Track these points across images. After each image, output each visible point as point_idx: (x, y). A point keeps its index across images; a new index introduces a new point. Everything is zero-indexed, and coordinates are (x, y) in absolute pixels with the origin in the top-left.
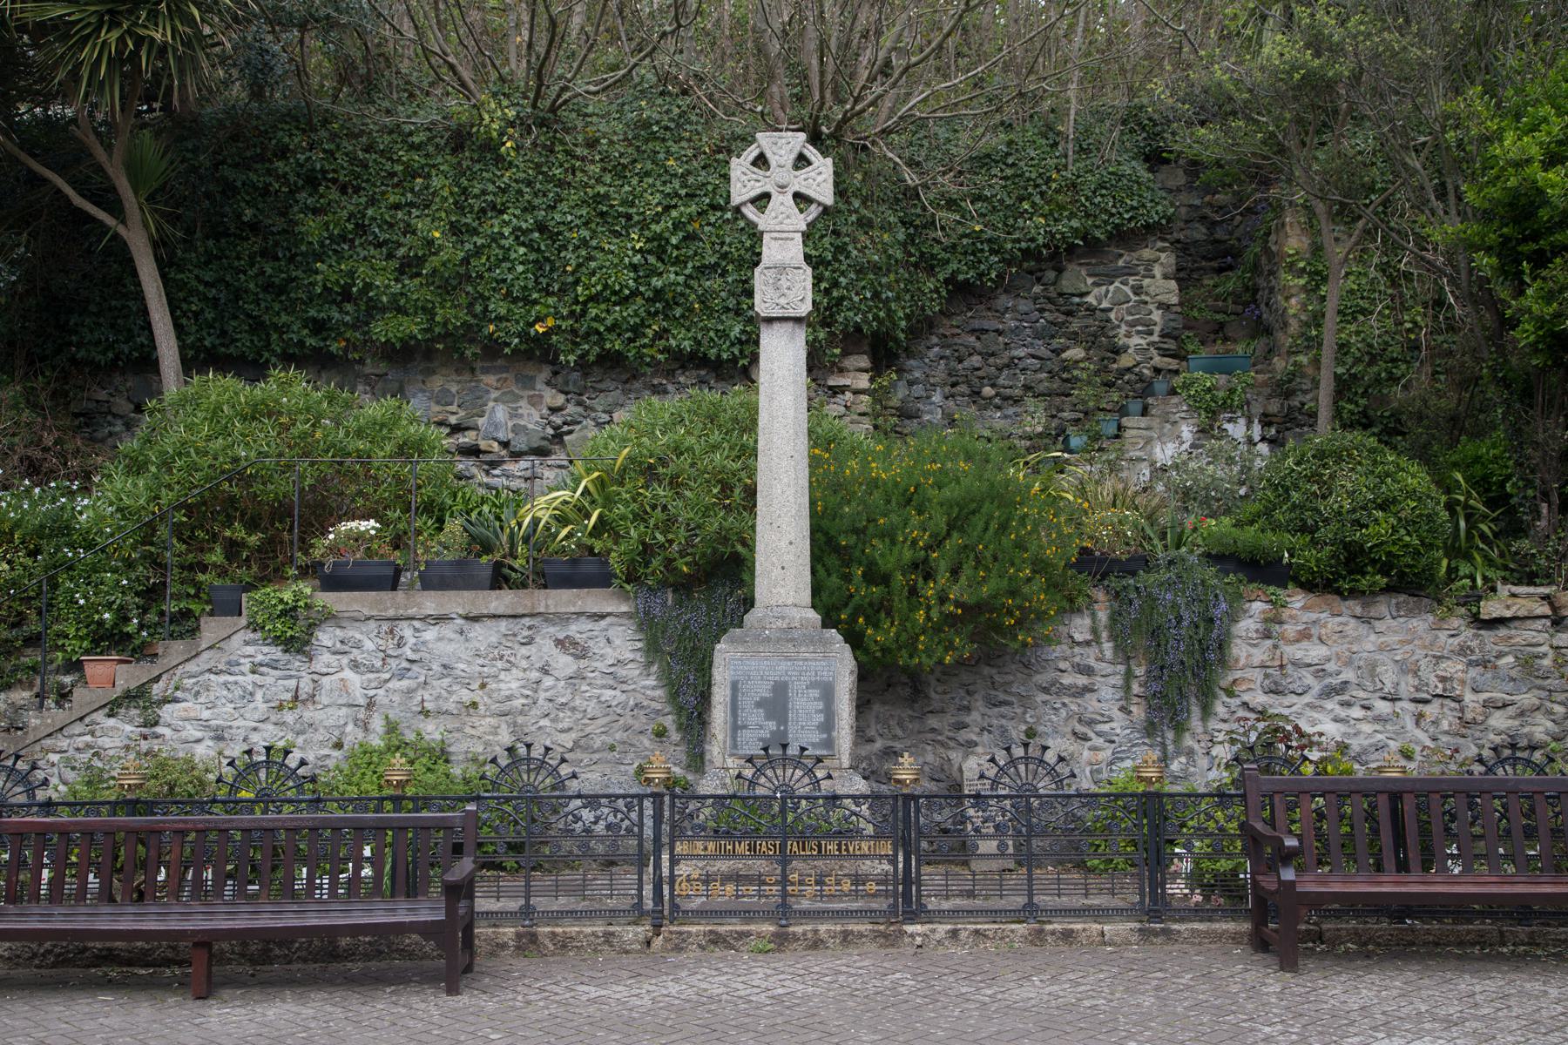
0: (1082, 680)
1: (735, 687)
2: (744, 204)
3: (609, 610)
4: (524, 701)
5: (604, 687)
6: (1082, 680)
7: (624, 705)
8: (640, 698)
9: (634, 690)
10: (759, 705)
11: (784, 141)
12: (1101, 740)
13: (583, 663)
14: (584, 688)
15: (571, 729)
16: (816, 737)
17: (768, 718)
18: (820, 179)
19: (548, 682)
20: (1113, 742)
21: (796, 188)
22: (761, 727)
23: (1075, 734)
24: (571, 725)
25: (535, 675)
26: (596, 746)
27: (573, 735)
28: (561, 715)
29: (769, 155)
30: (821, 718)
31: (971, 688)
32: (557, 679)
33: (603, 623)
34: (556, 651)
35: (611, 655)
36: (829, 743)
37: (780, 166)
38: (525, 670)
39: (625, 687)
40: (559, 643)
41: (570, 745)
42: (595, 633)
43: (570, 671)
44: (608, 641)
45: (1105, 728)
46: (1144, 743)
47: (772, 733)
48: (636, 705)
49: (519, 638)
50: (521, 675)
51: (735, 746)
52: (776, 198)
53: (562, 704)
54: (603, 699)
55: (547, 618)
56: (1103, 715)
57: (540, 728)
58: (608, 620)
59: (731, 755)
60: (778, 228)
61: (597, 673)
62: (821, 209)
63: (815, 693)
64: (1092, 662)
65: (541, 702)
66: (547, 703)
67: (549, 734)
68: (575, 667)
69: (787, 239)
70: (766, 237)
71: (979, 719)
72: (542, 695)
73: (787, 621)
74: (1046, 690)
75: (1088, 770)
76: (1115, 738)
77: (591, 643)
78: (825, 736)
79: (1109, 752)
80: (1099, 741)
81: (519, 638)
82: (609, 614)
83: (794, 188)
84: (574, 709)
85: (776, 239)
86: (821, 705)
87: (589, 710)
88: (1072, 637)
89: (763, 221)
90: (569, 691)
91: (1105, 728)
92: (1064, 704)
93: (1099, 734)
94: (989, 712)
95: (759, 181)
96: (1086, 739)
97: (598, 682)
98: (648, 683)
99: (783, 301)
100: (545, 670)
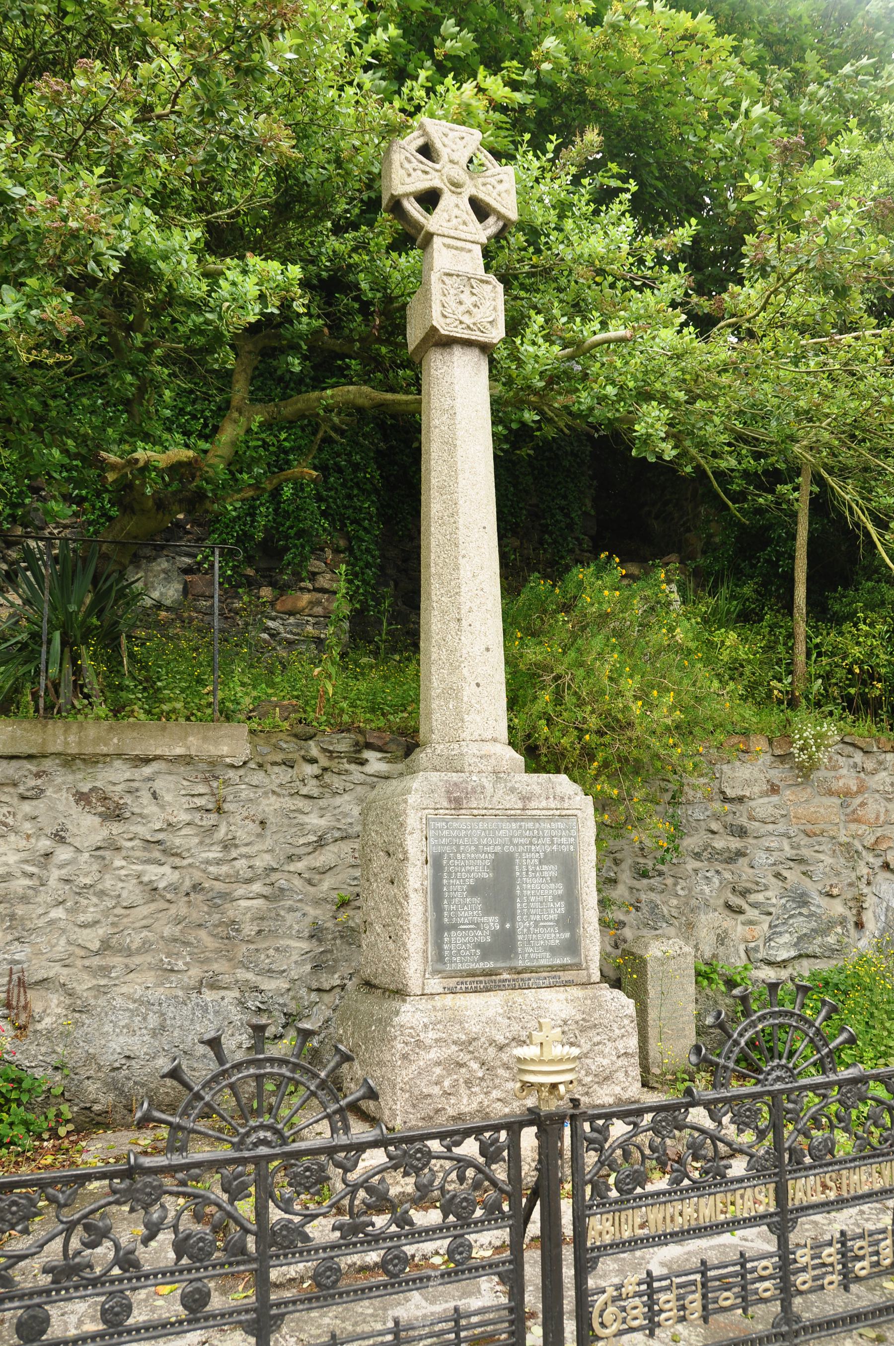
0: (735, 843)
1: (437, 864)
2: (407, 195)
3: (158, 752)
4: (28, 882)
5: (148, 861)
6: (735, 843)
7: (174, 888)
8: (198, 876)
9: (190, 865)
10: (473, 891)
11: (457, 134)
12: (756, 912)
13: (116, 828)
14: (118, 863)
15: (97, 922)
16: (557, 937)
17: (487, 912)
18: (500, 187)
19: (63, 854)
20: (770, 914)
21: (474, 192)
22: (478, 926)
23: (728, 906)
24: (98, 917)
25: (45, 844)
26: (134, 947)
27: (101, 931)
28: (84, 902)
29: (438, 145)
30: (560, 908)
31: (618, 855)
32: (78, 850)
33: (147, 770)
34: (75, 810)
35: (156, 817)
36: (572, 946)
37: (451, 161)
38: (28, 836)
39: (177, 861)
40: (82, 798)
41: (96, 945)
42: (135, 785)
43: (97, 838)
44: (155, 795)
45: (760, 897)
46: (800, 914)
47: (494, 934)
48: (194, 887)
49: (21, 789)
50: (23, 843)
51: (440, 957)
52: (447, 201)
53: (85, 886)
54: (146, 879)
55: (69, 761)
56: (757, 883)
57: (51, 922)
58: (155, 766)
59: (435, 972)
60: (452, 233)
61: (136, 842)
62: (501, 224)
63: (551, 870)
64: (744, 821)
65: (53, 882)
66: (61, 885)
67: (64, 931)
68: (105, 833)
69: (462, 249)
70: (437, 242)
71: (627, 894)
72: (55, 874)
73: (493, 761)
74: (697, 856)
75: (742, 948)
76: (772, 910)
77: (128, 799)
78: (567, 935)
79: (766, 926)
80: (752, 913)
81: (21, 789)
82: (156, 758)
83: (469, 190)
84: (102, 894)
85: (448, 247)
86: (559, 889)
87: (125, 894)
88: (723, 793)
89: (433, 222)
90: (95, 867)
91: (760, 897)
92: (717, 872)
93: (754, 905)
94: (637, 884)
95: (426, 173)
96: (741, 912)
97: (138, 854)
98: (211, 855)
99: (467, 320)
100: (59, 838)
